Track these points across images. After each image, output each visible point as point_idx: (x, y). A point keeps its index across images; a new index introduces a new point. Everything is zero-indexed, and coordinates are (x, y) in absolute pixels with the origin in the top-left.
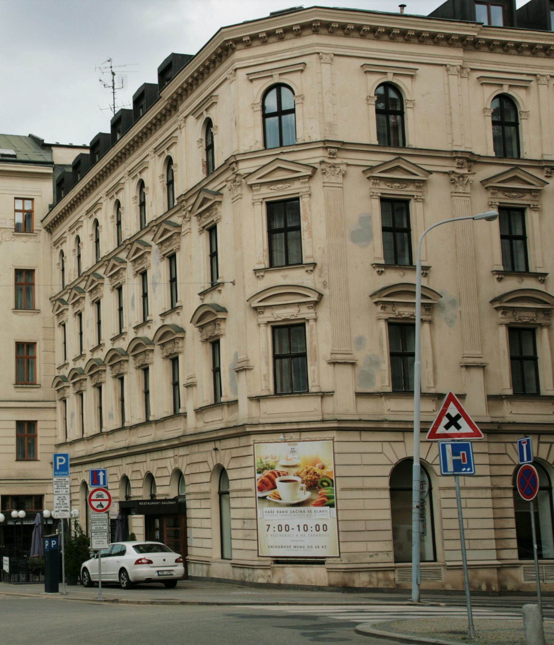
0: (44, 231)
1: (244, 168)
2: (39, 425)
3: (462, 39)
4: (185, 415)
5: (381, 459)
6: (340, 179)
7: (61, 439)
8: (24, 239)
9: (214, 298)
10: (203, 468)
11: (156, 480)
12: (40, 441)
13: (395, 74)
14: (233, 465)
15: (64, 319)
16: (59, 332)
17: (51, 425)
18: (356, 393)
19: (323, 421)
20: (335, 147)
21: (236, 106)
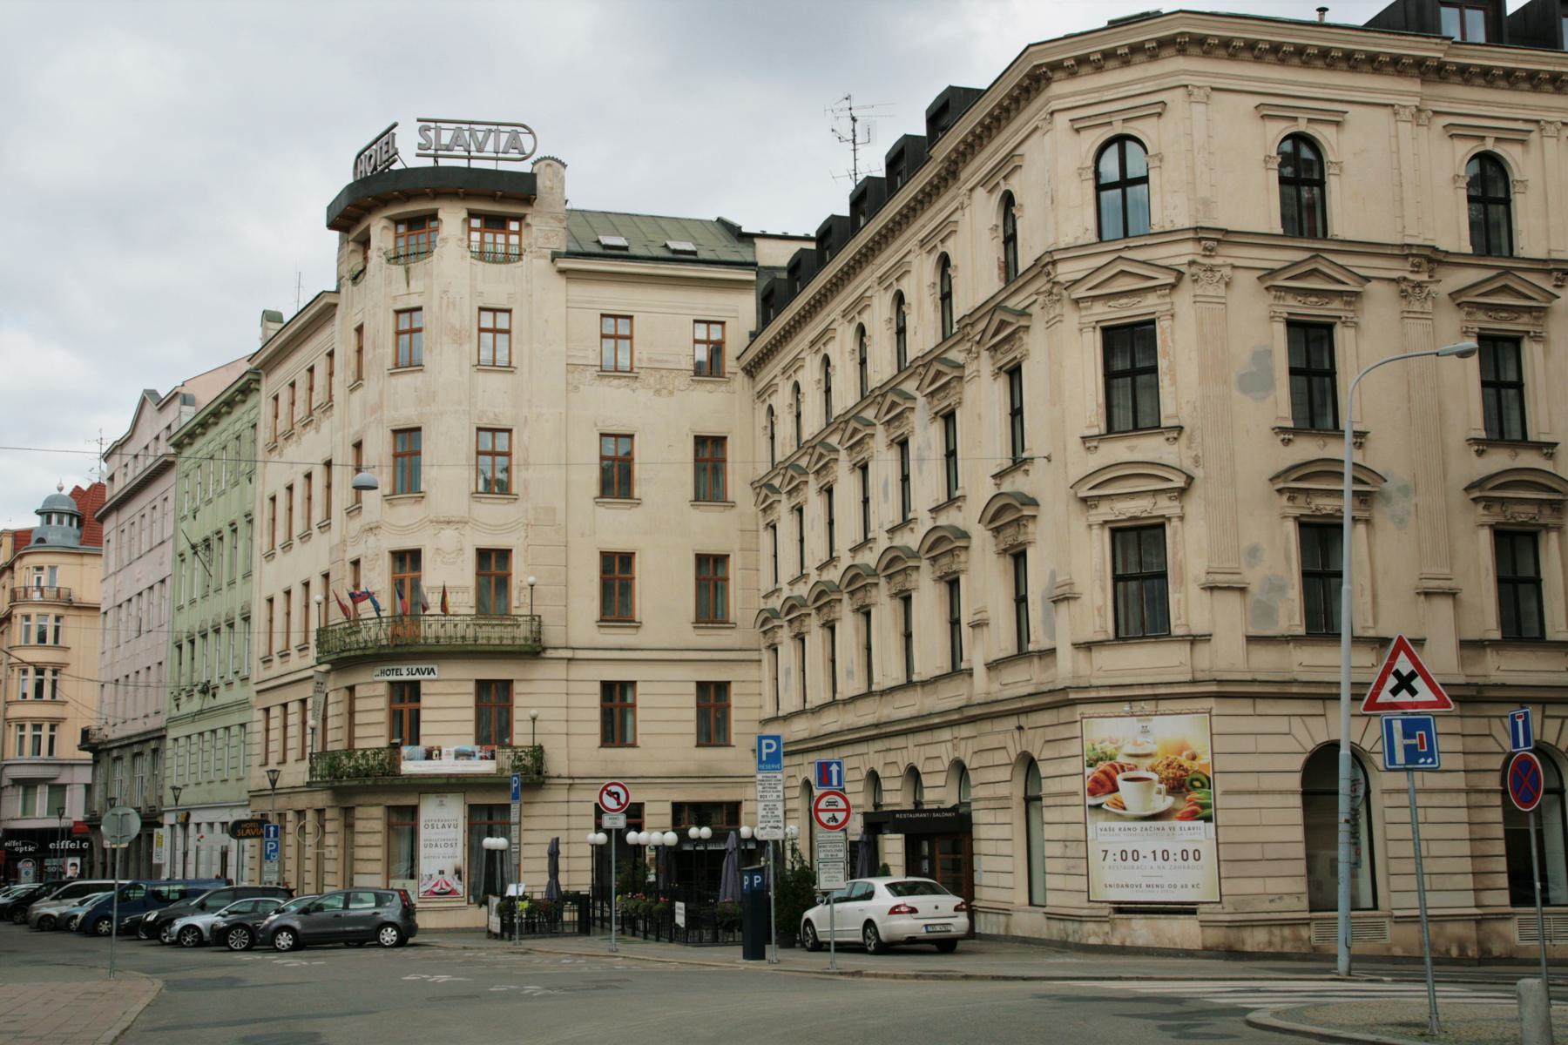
0: (741, 374)
1: (1065, 272)
2: (734, 689)
3: (1420, 63)
6: (1221, 290)
7: (769, 712)
8: (710, 387)
9: (1017, 483)
10: (1000, 757)
14: (1047, 754)
16: (766, 538)
17: (755, 688)
19: (1194, 682)
20: (1213, 238)
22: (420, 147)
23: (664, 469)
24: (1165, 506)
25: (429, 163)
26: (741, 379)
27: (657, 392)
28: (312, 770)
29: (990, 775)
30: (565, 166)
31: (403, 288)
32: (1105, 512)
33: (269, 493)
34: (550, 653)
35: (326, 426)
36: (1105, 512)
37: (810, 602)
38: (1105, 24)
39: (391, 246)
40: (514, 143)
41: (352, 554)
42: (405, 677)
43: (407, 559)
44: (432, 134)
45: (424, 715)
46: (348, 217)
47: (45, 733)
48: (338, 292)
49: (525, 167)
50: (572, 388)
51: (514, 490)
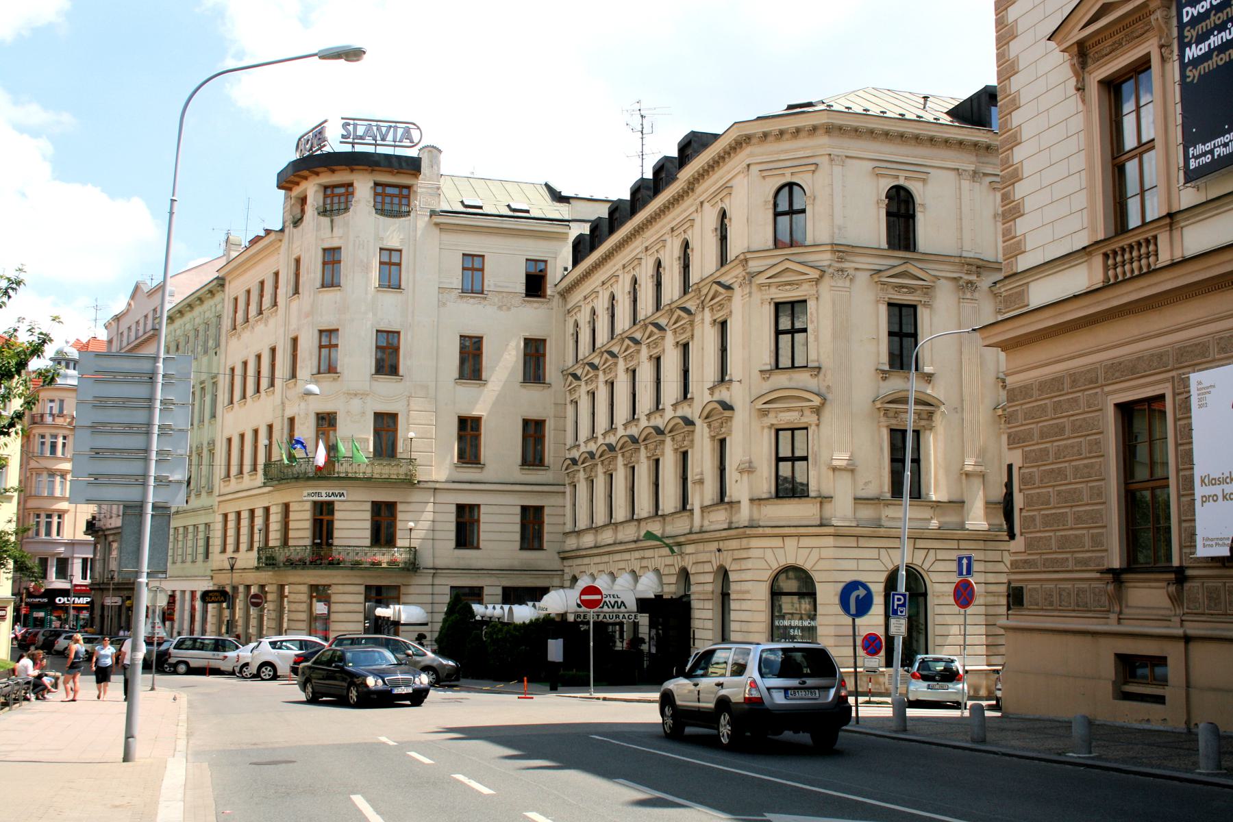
0: (557, 296)
1: (754, 266)
2: (546, 511)
3: (976, 144)
4: (692, 511)
5: (877, 565)
6: (848, 283)
7: (569, 527)
8: (535, 305)
9: (723, 394)
10: (708, 568)
11: (692, 577)
12: (546, 528)
13: (906, 178)
14: (734, 567)
15: (575, 396)
16: (570, 409)
17: (560, 511)
18: (855, 499)
19: (783, 536)
20: (842, 251)
21: (748, 200)
22: (343, 137)
23: (503, 362)
24: (810, 418)
25: (347, 148)
26: (557, 300)
27: (500, 308)
28: (259, 558)
29: (702, 579)
30: (440, 151)
31: (328, 233)
32: (772, 419)
33: (229, 364)
34: (422, 485)
35: (272, 322)
36: (772, 419)
37: (597, 456)
38: (780, 109)
39: (321, 203)
40: (407, 134)
41: (289, 414)
42: (324, 498)
43: (326, 421)
44: (351, 128)
45: (337, 524)
46: (289, 178)
47: (55, 520)
48: (282, 231)
49: (413, 153)
50: (442, 304)
51: (401, 373)
